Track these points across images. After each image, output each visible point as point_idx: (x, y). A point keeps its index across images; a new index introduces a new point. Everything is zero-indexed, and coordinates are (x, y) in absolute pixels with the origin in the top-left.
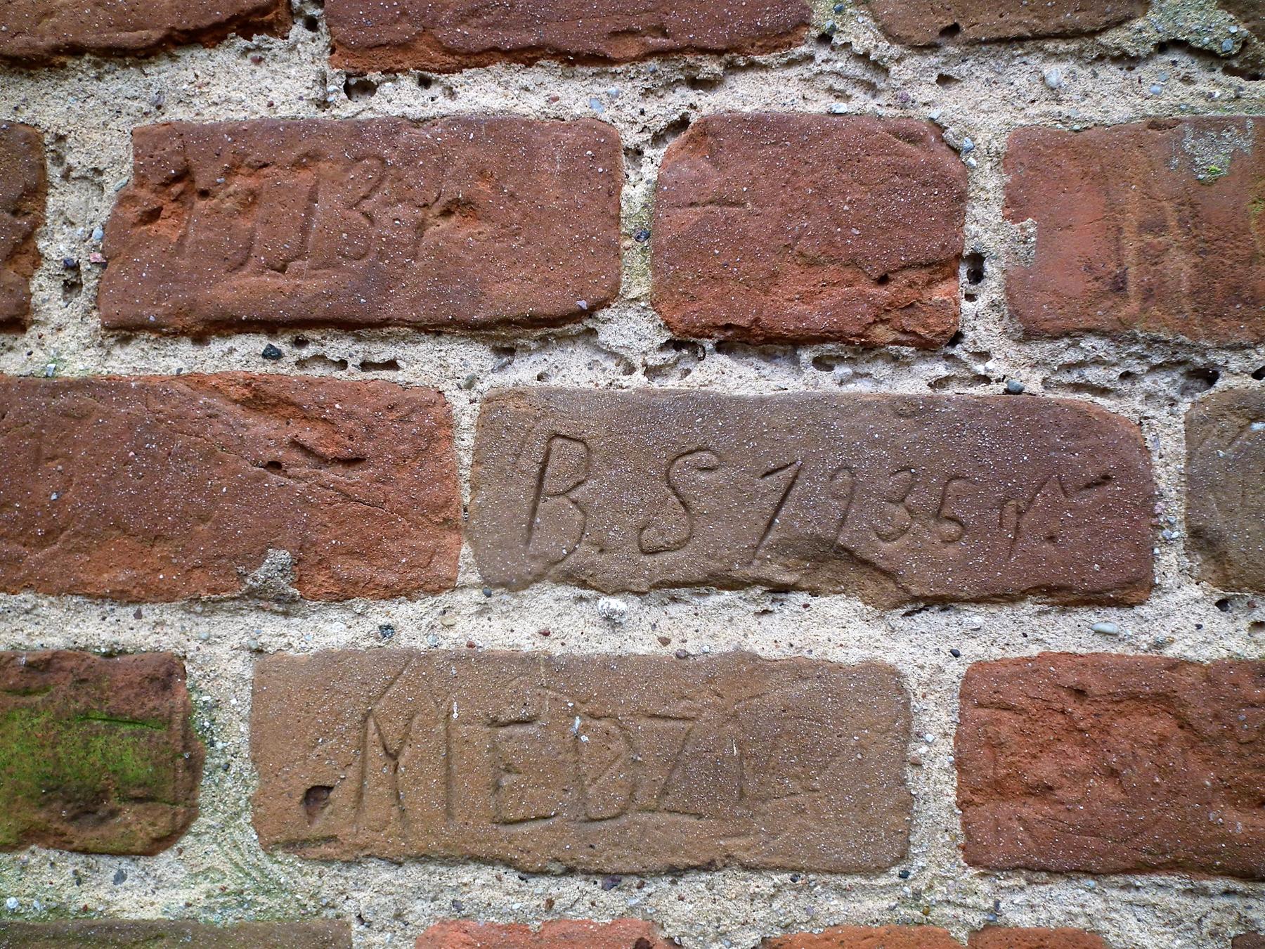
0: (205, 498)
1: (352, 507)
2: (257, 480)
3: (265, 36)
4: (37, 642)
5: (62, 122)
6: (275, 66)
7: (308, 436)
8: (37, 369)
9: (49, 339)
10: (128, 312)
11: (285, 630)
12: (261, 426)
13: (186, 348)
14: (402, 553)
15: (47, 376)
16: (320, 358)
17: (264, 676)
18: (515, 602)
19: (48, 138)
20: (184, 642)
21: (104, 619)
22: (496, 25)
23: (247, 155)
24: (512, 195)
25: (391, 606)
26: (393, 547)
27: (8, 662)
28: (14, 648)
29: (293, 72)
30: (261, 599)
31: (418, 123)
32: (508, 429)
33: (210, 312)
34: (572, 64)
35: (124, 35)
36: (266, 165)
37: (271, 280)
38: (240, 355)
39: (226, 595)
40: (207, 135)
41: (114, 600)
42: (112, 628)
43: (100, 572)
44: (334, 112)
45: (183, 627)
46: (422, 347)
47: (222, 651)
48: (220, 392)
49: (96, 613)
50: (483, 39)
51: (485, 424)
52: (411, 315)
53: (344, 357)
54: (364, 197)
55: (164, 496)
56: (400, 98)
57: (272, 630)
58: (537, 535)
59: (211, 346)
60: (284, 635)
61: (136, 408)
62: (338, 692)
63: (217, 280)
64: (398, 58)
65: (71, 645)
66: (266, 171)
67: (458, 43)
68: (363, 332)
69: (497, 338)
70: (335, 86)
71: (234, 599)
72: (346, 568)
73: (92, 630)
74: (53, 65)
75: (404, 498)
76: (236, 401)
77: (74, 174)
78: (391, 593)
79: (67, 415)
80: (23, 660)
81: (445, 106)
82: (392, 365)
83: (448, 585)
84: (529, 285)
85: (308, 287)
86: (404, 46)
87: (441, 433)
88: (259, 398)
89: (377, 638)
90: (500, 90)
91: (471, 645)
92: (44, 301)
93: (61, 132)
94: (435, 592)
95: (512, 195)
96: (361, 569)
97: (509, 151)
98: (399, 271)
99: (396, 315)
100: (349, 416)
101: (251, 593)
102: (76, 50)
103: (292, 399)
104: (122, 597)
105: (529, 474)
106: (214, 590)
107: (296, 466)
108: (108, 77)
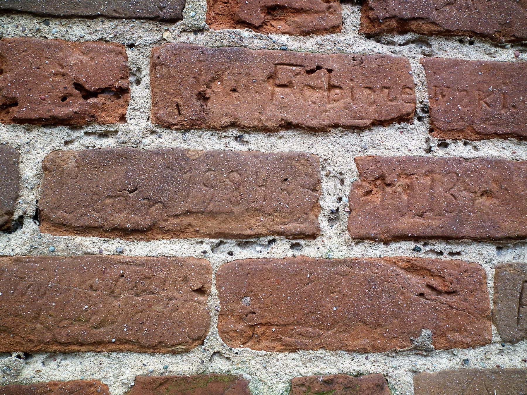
0: (398, 309)
1: (454, 311)
2: (417, 301)
3: (406, 123)
4: (326, 371)
5: (326, 154)
6: (409, 135)
7: (434, 282)
8: (323, 254)
9: (326, 242)
10: (363, 232)
11: (426, 363)
12: (415, 279)
13: (382, 246)
14: (472, 330)
15: (329, 258)
16: (432, 251)
17: (419, 382)
18: (513, 348)
19: (321, 160)
20: (387, 369)
21: (353, 360)
22: (496, 124)
23: (405, 170)
24: (506, 189)
25: (466, 351)
26: (469, 327)
27: (314, 381)
28: (315, 374)
29: (415, 137)
30: (418, 350)
31: (467, 160)
32: (508, 279)
33: (394, 232)
34: (521, 140)
35: (357, 121)
36: (412, 174)
37: (419, 220)
38: (403, 250)
39: (406, 349)
40: (389, 161)
41: (359, 352)
42: (357, 364)
43: (354, 340)
44: (435, 154)
45: (385, 363)
46: (472, 247)
47: (401, 372)
48: (396, 264)
49: (349, 358)
50: (491, 129)
51: (497, 277)
52: (472, 235)
53: (443, 251)
54: (451, 188)
55: (381, 308)
56: (458, 150)
57: (422, 363)
58: (521, 321)
59: (391, 245)
60: (425, 365)
61: (367, 272)
62: (450, 388)
63: (397, 219)
64: (459, 135)
65: (341, 372)
66: (413, 177)
67: (482, 130)
68: (451, 241)
69: (499, 243)
70: (434, 144)
71: (408, 350)
72: (451, 336)
73: (348, 365)
74: (327, 131)
75: (472, 307)
76: (403, 268)
77: (331, 175)
78: (468, 346)
79: (339, 275)
80: (321, 379)
81: (473, 154)
82: (459, 253)
83: (489, 342)
84: (516, 224)
85: (433, 223)
86: (462, 131)
87: (483, 281)
88: (413, 267)
89: (462, 365)
90: (495, 148)
91: (498, 367)
92: (324, 226)
93: (326, 157)
94: (483, 345)
95: (506, 189)
96: (457, 337)
97: (504, 172)
98: (467, 217)
99: (467, 235)
100: (450, 274)
101: (416, 348)
102: (336, 126)
103: (427, 268)
104: (364, 351)
105: (517, 297)
106: (401, 347)
107: (430, 295)
108: (345, 137)
